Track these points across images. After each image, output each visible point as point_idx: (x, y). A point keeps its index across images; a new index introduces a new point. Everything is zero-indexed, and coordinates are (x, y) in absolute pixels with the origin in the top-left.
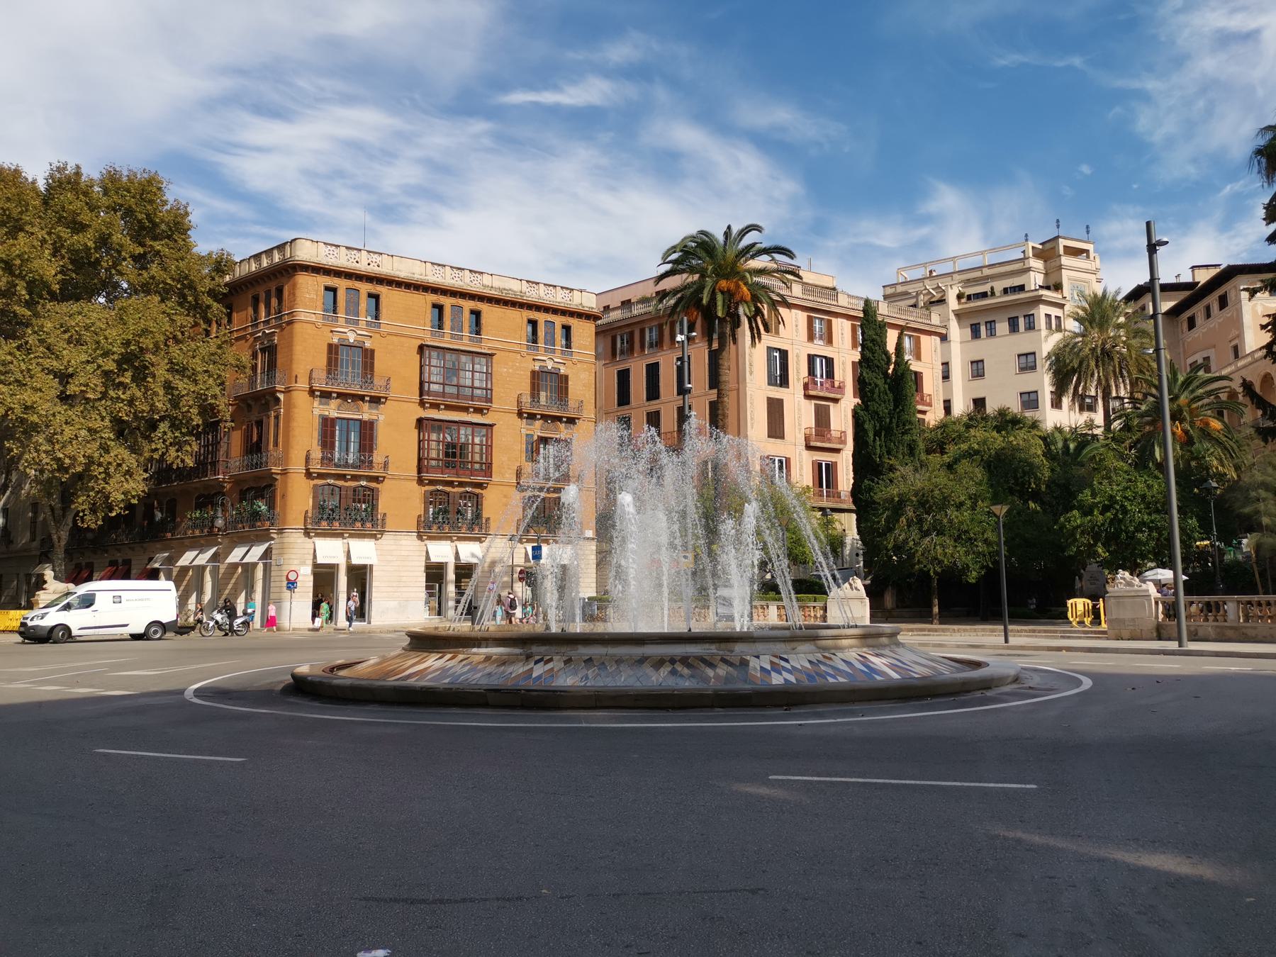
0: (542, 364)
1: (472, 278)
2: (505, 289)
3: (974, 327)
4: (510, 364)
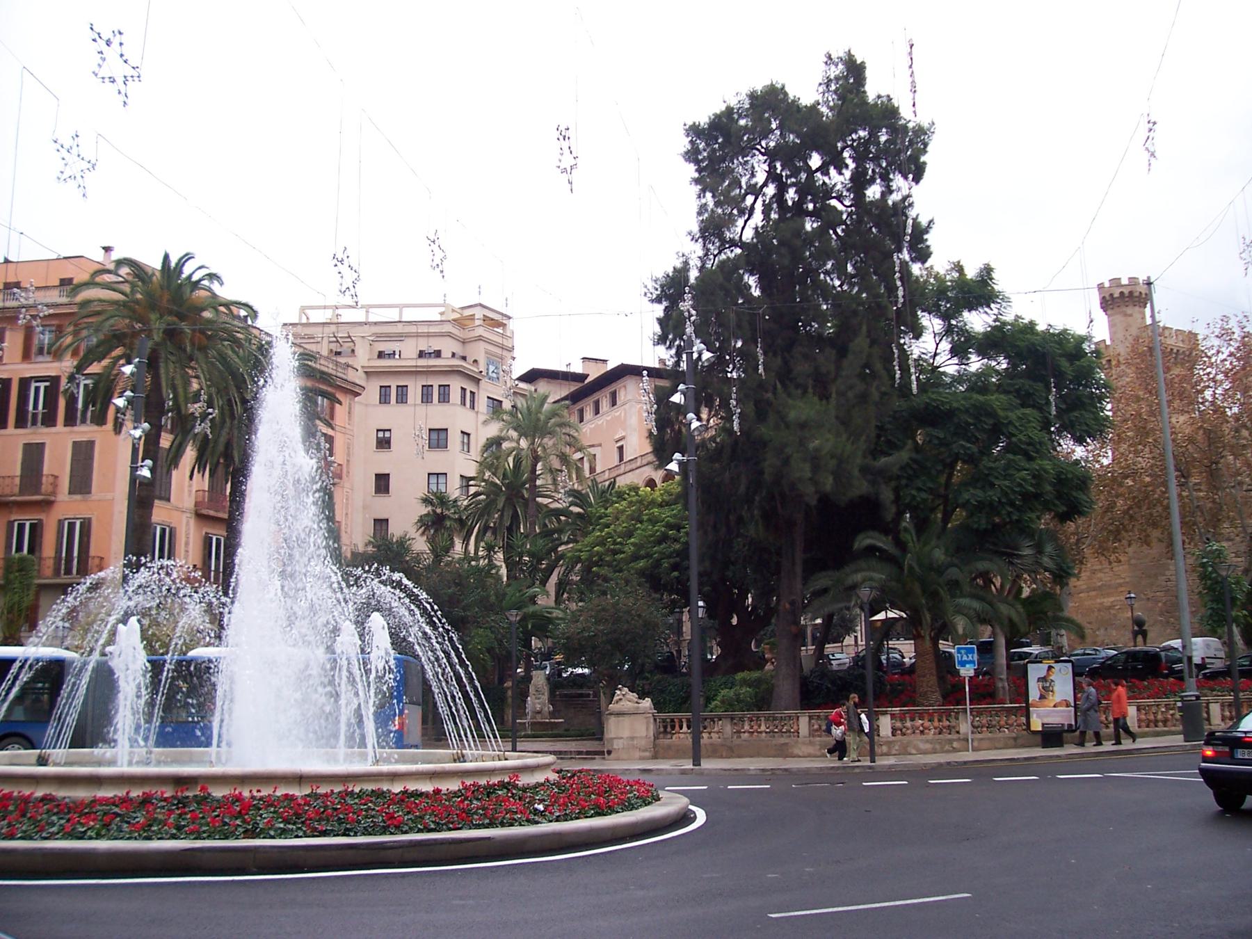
3: (383, 389)
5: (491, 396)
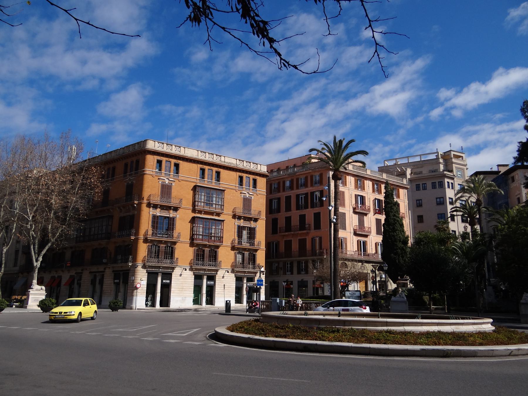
0: (163, 181)
1: (217, 158)
2: (230, 163)
4: (231, 194)
5: (328, 204)
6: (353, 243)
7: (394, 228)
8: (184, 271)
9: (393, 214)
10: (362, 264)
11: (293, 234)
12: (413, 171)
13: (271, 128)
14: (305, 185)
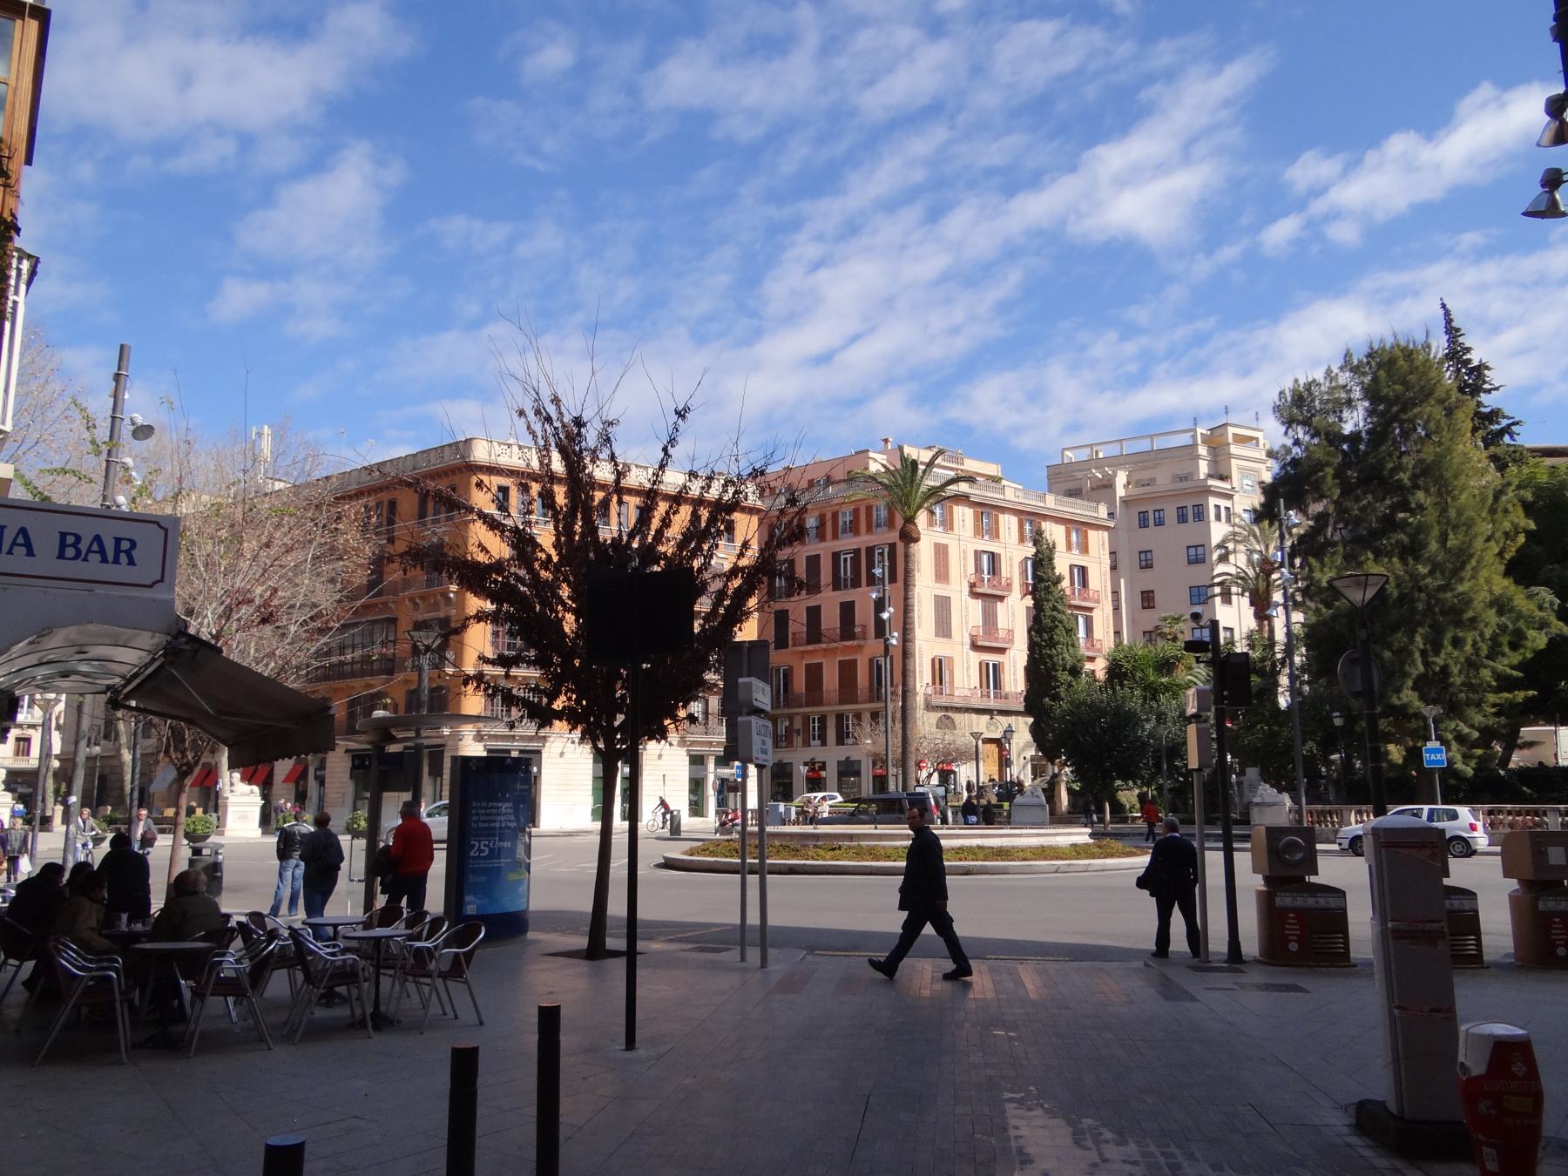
6: (968, 669)
7: (1051, 638)
8: (569, 744)
9: (1051, 605)
10: (991, 718)
11: (825, 650)
12: (1137, 476)
13: (779, 288)
14: (854, 528)
